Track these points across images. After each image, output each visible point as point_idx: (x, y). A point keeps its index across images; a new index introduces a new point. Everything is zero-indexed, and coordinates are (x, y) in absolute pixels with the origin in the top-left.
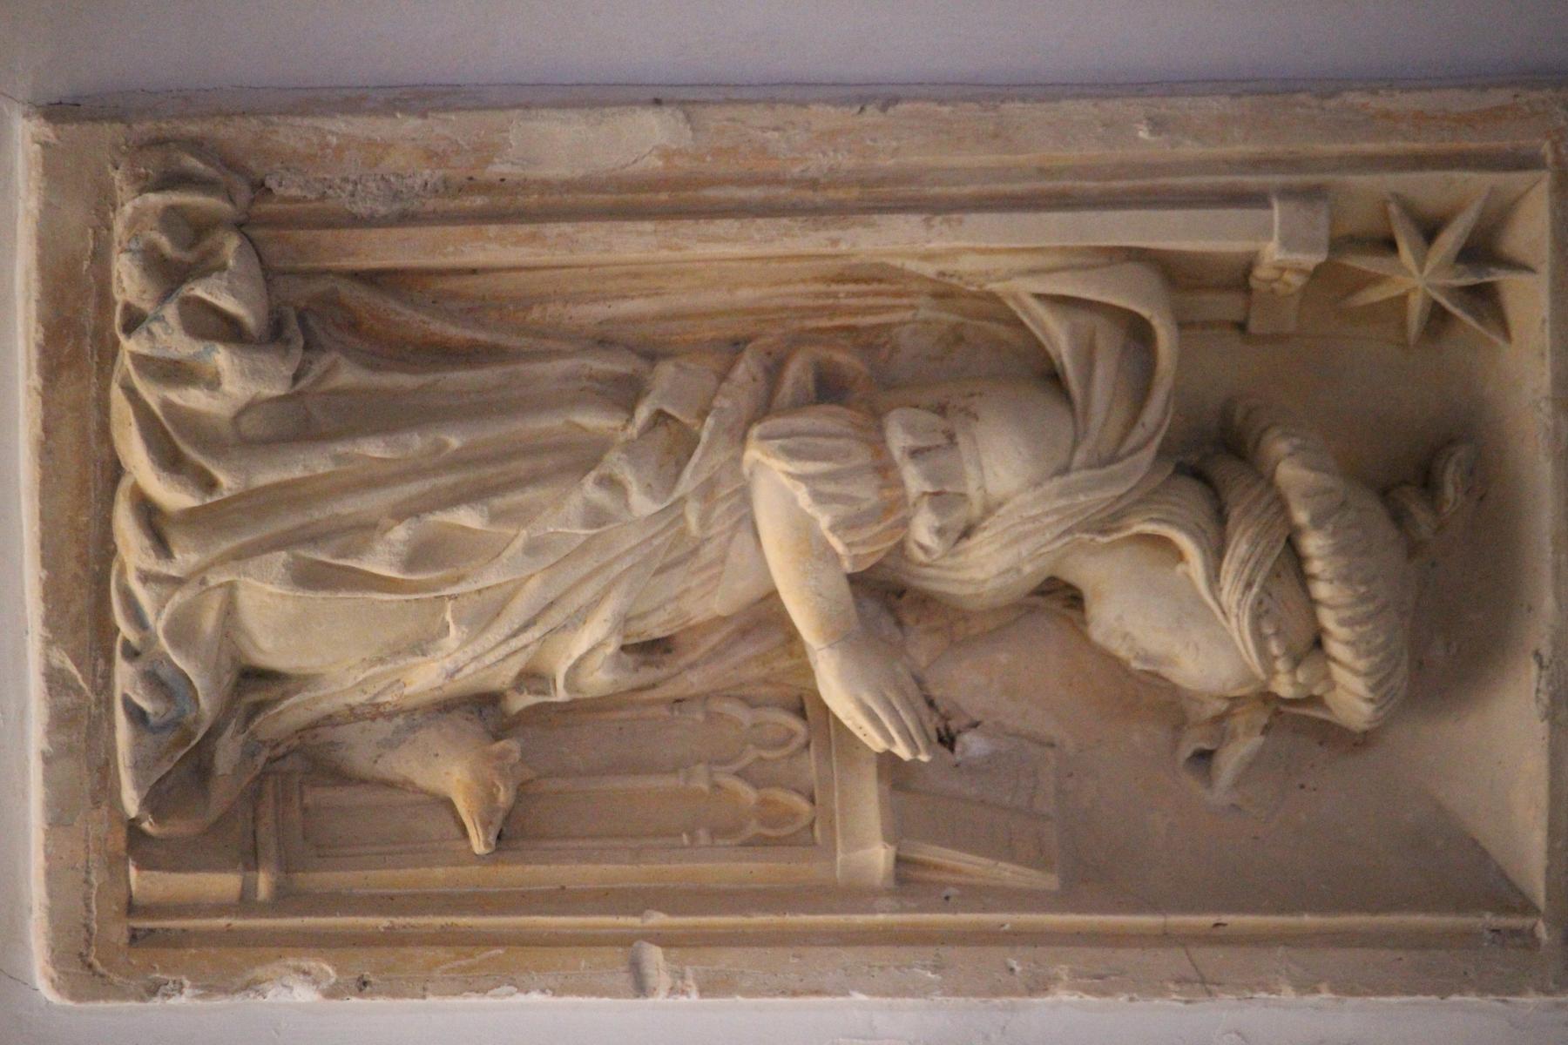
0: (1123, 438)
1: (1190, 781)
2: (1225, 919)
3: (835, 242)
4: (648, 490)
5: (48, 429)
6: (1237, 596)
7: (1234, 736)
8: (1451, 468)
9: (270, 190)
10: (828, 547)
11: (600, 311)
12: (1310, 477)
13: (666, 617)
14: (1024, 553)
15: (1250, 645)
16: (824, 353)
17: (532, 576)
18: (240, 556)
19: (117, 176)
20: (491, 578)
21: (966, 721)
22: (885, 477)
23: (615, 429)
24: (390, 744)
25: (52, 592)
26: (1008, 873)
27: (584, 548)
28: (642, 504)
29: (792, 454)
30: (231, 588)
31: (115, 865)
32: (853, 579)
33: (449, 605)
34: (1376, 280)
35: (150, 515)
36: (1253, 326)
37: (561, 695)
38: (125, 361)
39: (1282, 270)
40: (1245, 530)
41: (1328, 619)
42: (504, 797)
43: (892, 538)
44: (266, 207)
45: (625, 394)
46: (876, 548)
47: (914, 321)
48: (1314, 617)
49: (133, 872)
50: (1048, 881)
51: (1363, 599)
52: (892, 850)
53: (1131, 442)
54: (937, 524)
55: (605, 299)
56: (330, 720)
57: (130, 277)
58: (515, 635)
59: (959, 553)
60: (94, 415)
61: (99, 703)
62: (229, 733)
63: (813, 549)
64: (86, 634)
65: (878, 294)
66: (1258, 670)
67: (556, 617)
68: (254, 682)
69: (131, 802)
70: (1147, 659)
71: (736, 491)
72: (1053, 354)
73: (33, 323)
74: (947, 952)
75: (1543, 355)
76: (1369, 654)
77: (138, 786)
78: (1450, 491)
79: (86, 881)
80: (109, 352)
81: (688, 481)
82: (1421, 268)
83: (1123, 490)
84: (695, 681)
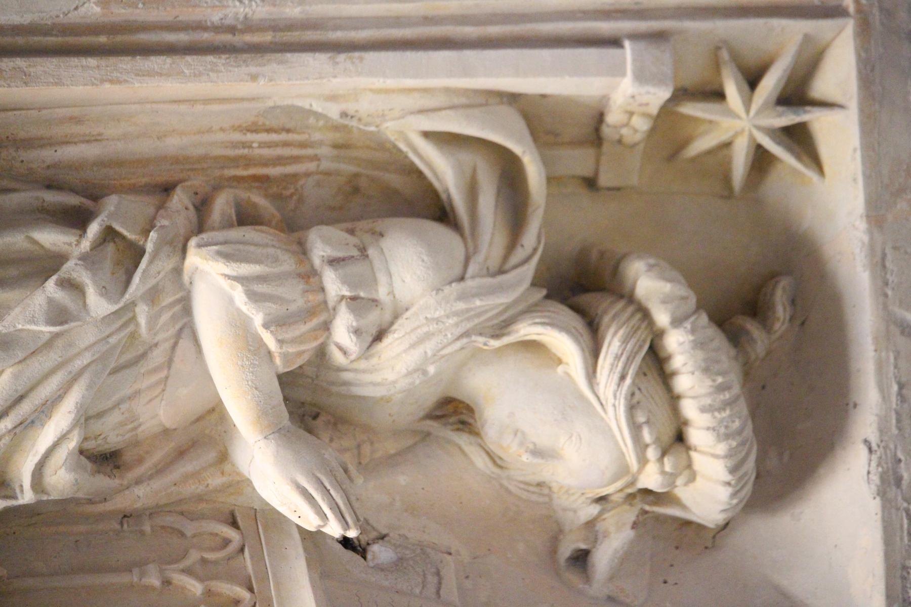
0: (506, 258)
1: (573, 577)
4: (104, 292)
6: (613, 386)
7: (606, 535)
8: (779, 293)
12: (667, 287)
14: (430, 353)
16: (244, 195)
22: (307, 283)
23: (70, 244)
27: (49, 344)
28: (98, 304)
29: (228, 257)
36: (604, 180)
37: (27, 497)
39: (631, 114)
40: (616, 333)
41: (689, 409)
43: (316, 339)
45: (77, 219)
47: (318, 173)
51: (721, 389)
53: (514, 259)
54: (354, 324)
55: (51, 145)
59: (372, 356)
63: (254, 348)
71: (179, 301)
75: (855, 180)
83: (504, 299)
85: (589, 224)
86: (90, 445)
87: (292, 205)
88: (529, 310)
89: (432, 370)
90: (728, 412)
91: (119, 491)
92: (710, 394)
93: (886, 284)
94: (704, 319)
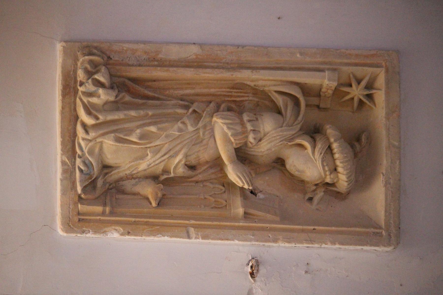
1: (308, 204)
2: (316, 227)
3: (232, 75)
4: (192, 125)
5: (63, 108)
6: (318, 156)
9: (111, 59)
10: (230, 140)
11: (181, 92)
13: (195, 157)
15: (322, 169)
16: (230, 104)
17: (166, 143)
18: (103, 135)
19: (79, 53)
20: (158, 143)
21: (259, 191)
24: (134, 185)
25: (63, 143)
26: (269, 216)
28: (190, 128)
29: (223, 118)
30: (101, 143)
31: (75, 204)
32: (236, 149)
33: (149, 149)
34: (348, 93)
35: (84, 126)
36: (321, 106)
37: (172, 175)
38: (80, 93)
39: (328, 89)
41: (338, 163)
42: (160, 195)
44: (111, 62)
45: (187, 107)
46: (241, 142)
48: (335, 163)
49: (79, 205)
50: (278, 219)
52: (244, 209)
56: (121, 179)
57: (81, 74)
58: (162, 156)
60: (73, 106)
61: (73, 168)
62: (100, 178)
63: (227, 140)
64: (70, 153)
65: (241, 92)
66: (323, 174)
67: (171, 153)
68: (106, 168)
69: (79, 189)
70: (298, 171)
71: (210, 129)
72: (279, 105)
73: (60, 85)
74: (255, 232)
75: (383, 108)
76: (347, 170)
77: (81, 186)
78: (363, 140)
79: (69, 207)
80: (76, 92)
81: (200, 124)
82: (357, 89)
83: (294, 132)
84: (200, 177)
85: (315, 116)
86: (187, 163)
87: (242, 108)
88: (298, 137)
89: (273, 149)
90: (347, 164)
91: (195, 176)
92: (275, 129)
93: (389, 134)
94: (343, 140)
